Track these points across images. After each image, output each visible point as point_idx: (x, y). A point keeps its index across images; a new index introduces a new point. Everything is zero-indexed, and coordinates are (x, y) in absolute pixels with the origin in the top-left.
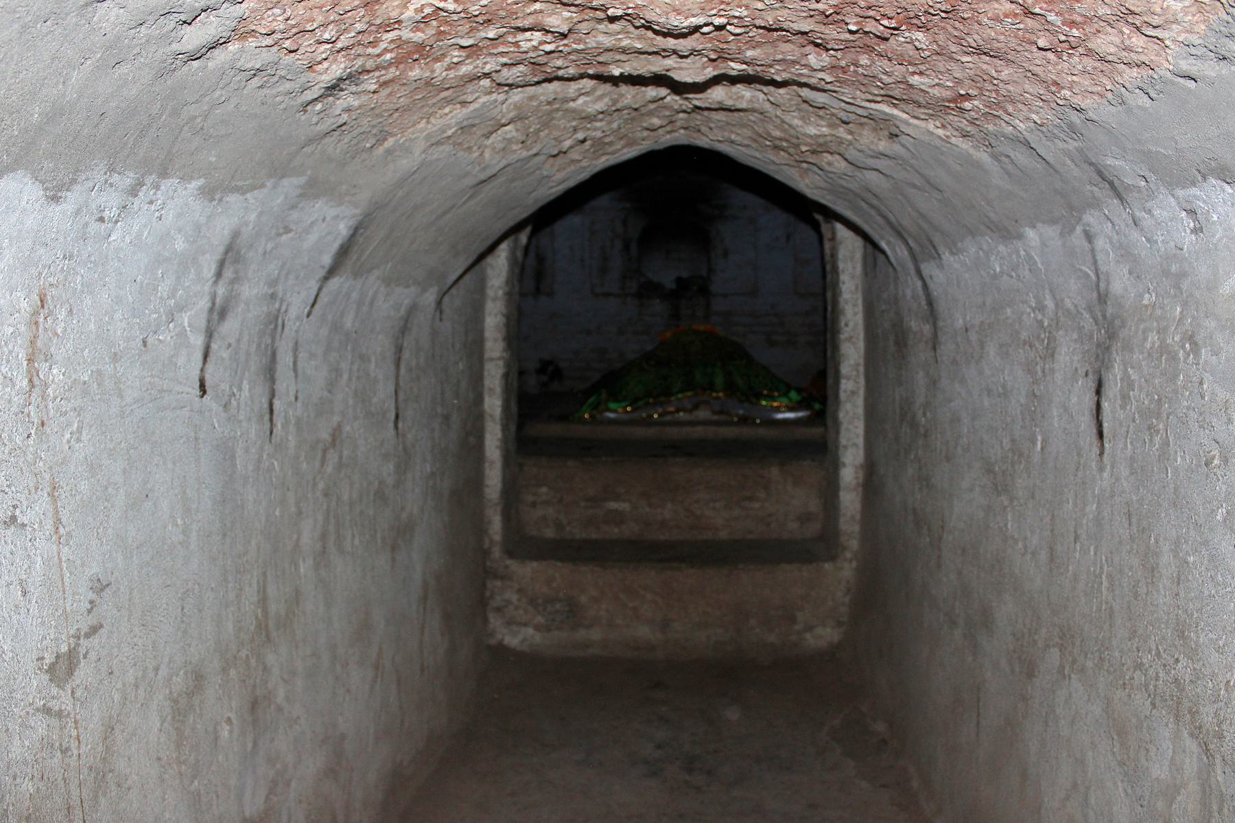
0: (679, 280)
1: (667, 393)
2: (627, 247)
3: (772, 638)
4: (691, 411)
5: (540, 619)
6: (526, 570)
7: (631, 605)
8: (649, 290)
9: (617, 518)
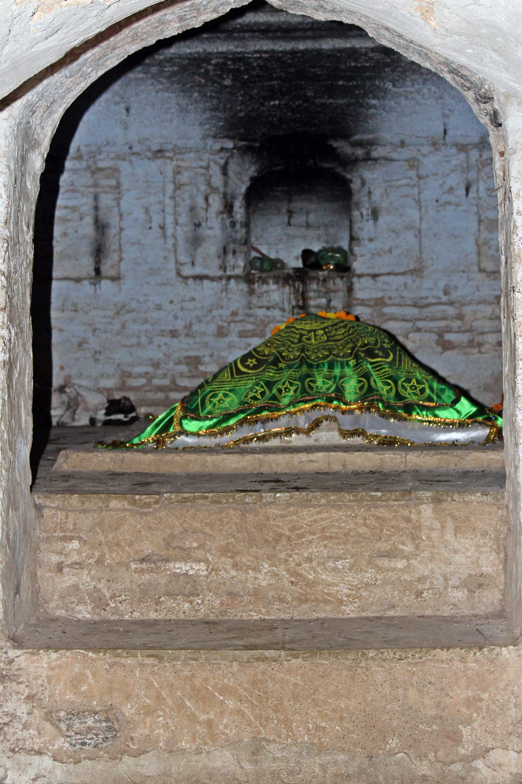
0: (307, 254)
1: (273, 405)
2: (228, 208)
3: (423, 768)
4: (307, 432)
5: (61, 743)
6: (39, 666)
7: (203, 717)
8: (261, 269)
9: (190, 588)
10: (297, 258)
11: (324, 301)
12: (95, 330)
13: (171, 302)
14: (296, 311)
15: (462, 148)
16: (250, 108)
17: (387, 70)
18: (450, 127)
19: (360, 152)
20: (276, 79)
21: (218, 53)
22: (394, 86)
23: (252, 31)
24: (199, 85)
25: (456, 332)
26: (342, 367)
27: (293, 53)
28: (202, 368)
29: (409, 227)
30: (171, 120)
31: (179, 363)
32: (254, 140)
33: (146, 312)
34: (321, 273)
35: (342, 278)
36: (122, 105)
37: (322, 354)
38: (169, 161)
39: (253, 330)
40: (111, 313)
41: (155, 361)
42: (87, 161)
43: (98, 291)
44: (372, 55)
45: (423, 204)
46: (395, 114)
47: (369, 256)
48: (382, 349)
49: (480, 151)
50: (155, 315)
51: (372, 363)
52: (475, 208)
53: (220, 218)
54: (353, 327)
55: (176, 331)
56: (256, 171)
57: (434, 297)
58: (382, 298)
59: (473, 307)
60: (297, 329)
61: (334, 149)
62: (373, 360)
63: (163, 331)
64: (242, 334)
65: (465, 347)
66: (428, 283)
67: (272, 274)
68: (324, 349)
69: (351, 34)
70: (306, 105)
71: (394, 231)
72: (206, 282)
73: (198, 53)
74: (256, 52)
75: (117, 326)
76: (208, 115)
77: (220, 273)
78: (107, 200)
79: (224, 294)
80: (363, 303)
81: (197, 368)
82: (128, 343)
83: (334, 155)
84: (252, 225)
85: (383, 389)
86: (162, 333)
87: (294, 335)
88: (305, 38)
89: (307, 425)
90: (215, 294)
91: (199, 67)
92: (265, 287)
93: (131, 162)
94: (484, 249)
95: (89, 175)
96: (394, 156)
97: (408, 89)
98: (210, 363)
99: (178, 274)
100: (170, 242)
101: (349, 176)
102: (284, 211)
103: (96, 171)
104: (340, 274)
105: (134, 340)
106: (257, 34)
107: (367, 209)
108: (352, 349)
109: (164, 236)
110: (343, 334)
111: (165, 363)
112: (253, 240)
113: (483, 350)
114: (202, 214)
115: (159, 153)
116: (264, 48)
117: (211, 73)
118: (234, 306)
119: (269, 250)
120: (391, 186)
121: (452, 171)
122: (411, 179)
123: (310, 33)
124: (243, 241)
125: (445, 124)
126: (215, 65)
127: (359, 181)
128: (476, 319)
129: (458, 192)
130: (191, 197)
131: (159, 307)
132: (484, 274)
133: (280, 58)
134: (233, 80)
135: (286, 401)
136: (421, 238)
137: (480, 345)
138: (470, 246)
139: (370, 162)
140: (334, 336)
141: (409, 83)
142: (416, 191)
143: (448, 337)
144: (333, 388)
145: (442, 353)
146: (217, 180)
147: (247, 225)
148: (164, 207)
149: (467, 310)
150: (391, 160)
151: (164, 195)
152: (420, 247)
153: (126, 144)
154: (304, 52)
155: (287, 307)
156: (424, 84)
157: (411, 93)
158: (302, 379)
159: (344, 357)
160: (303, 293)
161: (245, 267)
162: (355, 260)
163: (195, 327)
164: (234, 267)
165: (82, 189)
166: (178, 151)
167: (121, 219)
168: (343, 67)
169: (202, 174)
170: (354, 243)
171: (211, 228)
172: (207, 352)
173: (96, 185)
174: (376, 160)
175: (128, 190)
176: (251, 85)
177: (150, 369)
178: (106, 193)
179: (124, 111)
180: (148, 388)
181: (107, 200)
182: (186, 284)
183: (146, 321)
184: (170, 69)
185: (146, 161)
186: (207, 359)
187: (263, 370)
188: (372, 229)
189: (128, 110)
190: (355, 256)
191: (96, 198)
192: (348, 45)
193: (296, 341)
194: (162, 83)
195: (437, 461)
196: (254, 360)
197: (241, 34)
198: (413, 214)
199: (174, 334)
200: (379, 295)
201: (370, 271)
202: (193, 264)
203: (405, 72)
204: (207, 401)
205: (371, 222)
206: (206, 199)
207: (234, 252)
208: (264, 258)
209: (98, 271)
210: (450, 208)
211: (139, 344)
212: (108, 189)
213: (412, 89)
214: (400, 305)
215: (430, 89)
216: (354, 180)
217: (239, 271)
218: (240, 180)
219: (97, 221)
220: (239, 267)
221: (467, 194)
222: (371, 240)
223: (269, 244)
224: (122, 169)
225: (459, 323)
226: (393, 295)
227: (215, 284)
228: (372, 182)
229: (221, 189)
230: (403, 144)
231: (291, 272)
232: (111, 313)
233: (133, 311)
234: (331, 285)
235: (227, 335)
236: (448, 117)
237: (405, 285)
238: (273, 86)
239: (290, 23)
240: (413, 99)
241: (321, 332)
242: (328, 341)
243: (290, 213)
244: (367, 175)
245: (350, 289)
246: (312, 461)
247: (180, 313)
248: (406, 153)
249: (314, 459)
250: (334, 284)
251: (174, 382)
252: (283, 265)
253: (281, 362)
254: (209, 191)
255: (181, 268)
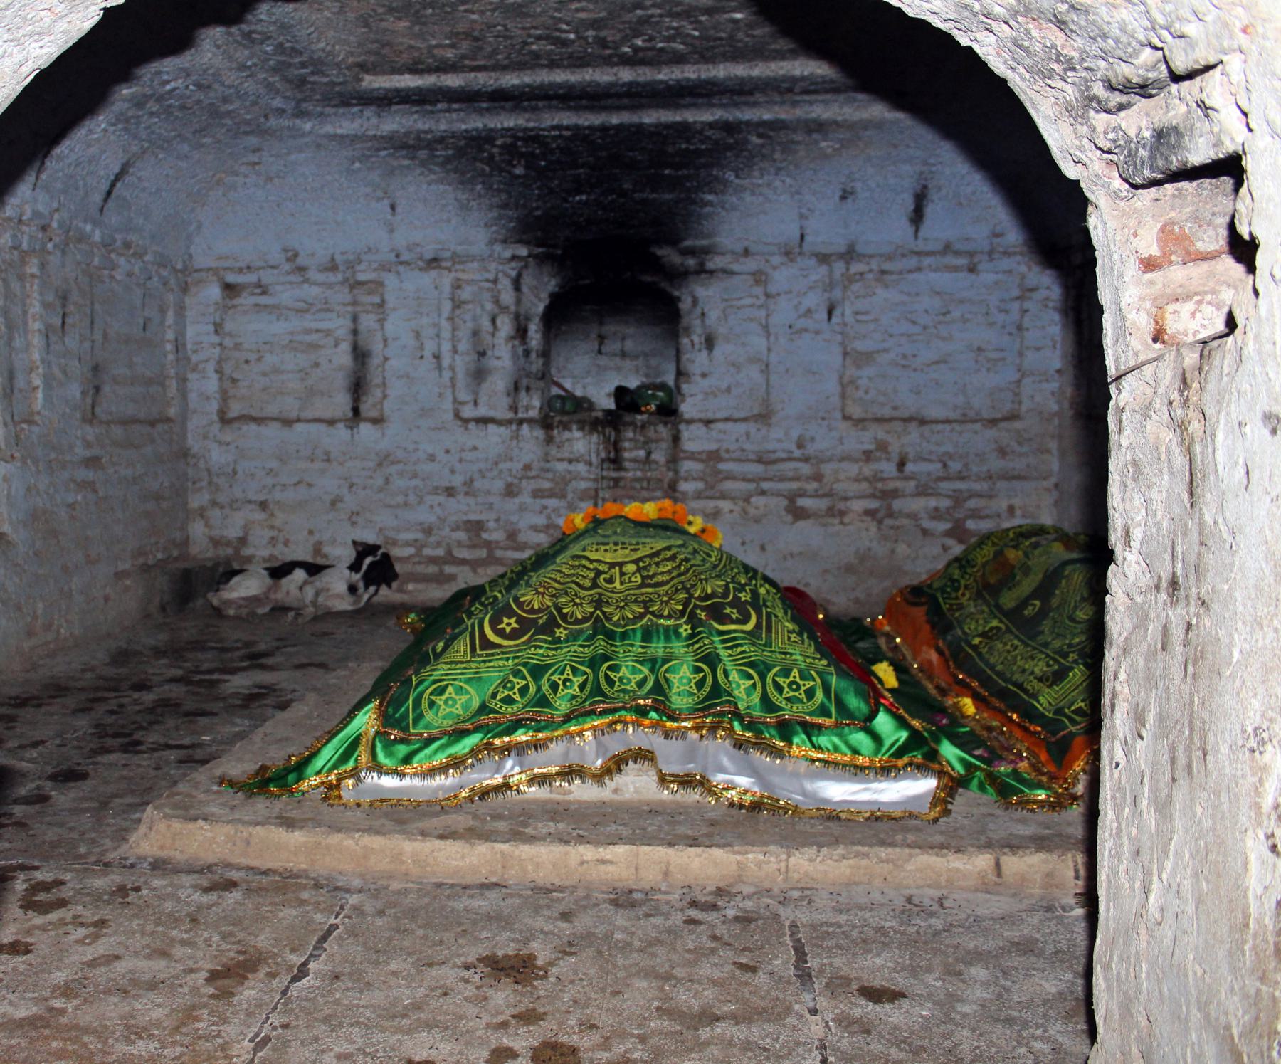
0: (620, 392)
2: (521, 332)
8: (565, 411)
10: (609, 395)
11: (642, 453)
12: (352, 485)
13: (447, 452)
14: (605, 466)
15: (824, 259)
16: (549, 205)
17: (729, 154)
18: (808, 231)
19: (691, 262)
20: (582, 166)
21: (503, 129)
22: (737, 176)
23: (547, 97)
24: (482, 173)
25: (810, 496)
26: (667, 639)
27: (604, 129)
28: (485, 536)
29: (753, 360)
30: (449, 221)
31: (456, 528)
32: (554, 246)
33: (415, 464)
34: (639, 417)
35: (666, 424)
36: (386, 202)
37: (632, 611)
38: (446, 272)
39: (551, 489)
40: (371, 464)
41: (426, 526)
42: (344, 272)
43: (356, 436)
44: (709, 133)
45: (772, 330)
46: (738, 213)
47: (700, 397)
48: (736, 603)
49: (848, 263)
50: (428, 467)
51: (721, 633)
52: (839, 337)
53: (510, 345)
54: (687, 560)
55: (453, 488)
56: (557, 285)
57: (783, 451)
58: (717, 451)
59: (834, 465)
60: (591, 561)
61: (658, 258)
62: (721, 628)
63: (437, 488)
64: (537, 494)
65: (823, 516)
66: (777, 433)
67: (577, 417)
68: (636, 601)
69: (682, 102)
70: (622, 200)
71: (733, 365)
72: (492, 427)
73: (476, 129)
74: (554, 128)
75: (380, 481)
76: (495, 214)
77: (510, 415)
78: (368, 321)
79: (515, 442)
80: (692, 456)
81: (479, 536)
82: (393, 503)
83: (657, 266)
84: (553, 353)
85: (739, 686)
86: (435, 491)
87: (585, 573)
88: (619, 108)
89: (599, 763)
90: (503, 442)
91: (481, 150)
92: (567, 435)
93: (398, 273)
94: (850, 390)
95: (347, 290)
96: (735, 267)
97: (754, 181)
98: (496, 530)
99: (457, 415)
100: (447, 375)
101: (676, 293)
102: (593, 336)
103: (355, 285)
104: (664, 419)
105: (400, 499)
106: (555, 102)
107: (700, 336)
108: (686, 603)
109: (439, 367)
110: (669, 572)
111: (439, 529)
112: (553, 371)
113: (846, 520)
114: (487, 339)
115: (434, 263)
116: (565, 123)
117: (497, 159)
118: (527, 459)
119: (573, 384)
120: (731, 306)
121: (811, 288)
122: (757, 297)
123: (626, 101)
124: (540, 375)
125: (801, 228)
126: (501, 147)
127: (689, 300)
128: (838, 480)
129: (816, 316)
130: (474, 319)
131: (432, 458)
132: (849, 423)
133: (586, 136)
134: (526, 167)
135: (562, 705)
136: (768, 374)
137: (842, 513)
138: (832, 386)
139: (703, 276)
140: (655, 575)
141: (756, 173)
142: (763, 313)
143: (801, 502)
144: (650, 684)
145: (793, 523)
146: (508, 297)
147: (545, 354)
148: (439, 331)
149: (827, 469)
150: (732, 273)
151: (439, 315)
152: (768, 385)
153: (392, 250)
154: (619, 128)
155: (594, 460)
156: (777, 174)
157: (759, 186)
158: (594, 663)
159: (669, 617)
160: (616, 444)
161: (541, 408)
162: (683, 401)
163: (477, 484)
164: (527, 408)
165: (338, 308)
166: (457, 259)
167: (385, 346)
168: (670, 149)
169: (488, 289)
170: (682, 379)
171: (498, 358)
172: (493, 516)
173: (354, 303)
174: (711, 272)
175: (394, 309)
176: (550, 174)
177: (420, 536)
178: (367, 312)
179: (389, 209)
180: (417, 559)
181: (368, 321)
182: (466, 429)
183: (415, 476)
184: (443, 153)
185: (417, 272)
186: (492, 524)
187: (529, 640)
188: (706, 362)
189: (393, 207)
190: (683, 395)
191: (355, 319)
192: (678, 119)
193: (588, 584)
194: (435, 173)
195: (848, 871)
196: (513, 620)
197: (534, 103)
198: (759, 343)
199: (450, 492)
200: (714, 447)
201: (702, 416)
202: (476, 403)
203: (754, 157)
204: (425, 703)
205: (705, 353)
206: (493, 321)
207: (528, 389)
208: (569, 396)
209: (356, 411)
210: (807, 336)
211: (406, 504)
212: (370, 308)
213: (760, 182)
214: (739, 460)
215: (783, 182)
216: (683, 297)
217: (533, 413)
218: (537, 296)
219: (355, 348)
220: (534, 407)
221: (829, 318)
222: (704, 375)
223: (574, 377)
224: (387, 282)
225: (815, 485)
226: (732, 447)
227: (502, 429)
228: (707, 301)
229: (513, 308)
230: (746, 252)
231: (600, 414)
232: (371, 464)
233: (399, 462)
234: (651, 433)
235: (517, 495)
236: (807, 218)
237: (748, 435)
238: (579, 175)
239: (598, 84)
240: (761, 194)
241: (631, 568)
242: (642, 586)
243: (602, 339)
244: (701, 292)
245: (676, 439)
246: (603, 862)
247: (458, 467)
248: (751, 264)
249: (609, 857)
250: (656, 431)
251: (449, 552)
252: (591, 406)
253: (559, 626)
254: (496, 310)
255: (460, 407)
